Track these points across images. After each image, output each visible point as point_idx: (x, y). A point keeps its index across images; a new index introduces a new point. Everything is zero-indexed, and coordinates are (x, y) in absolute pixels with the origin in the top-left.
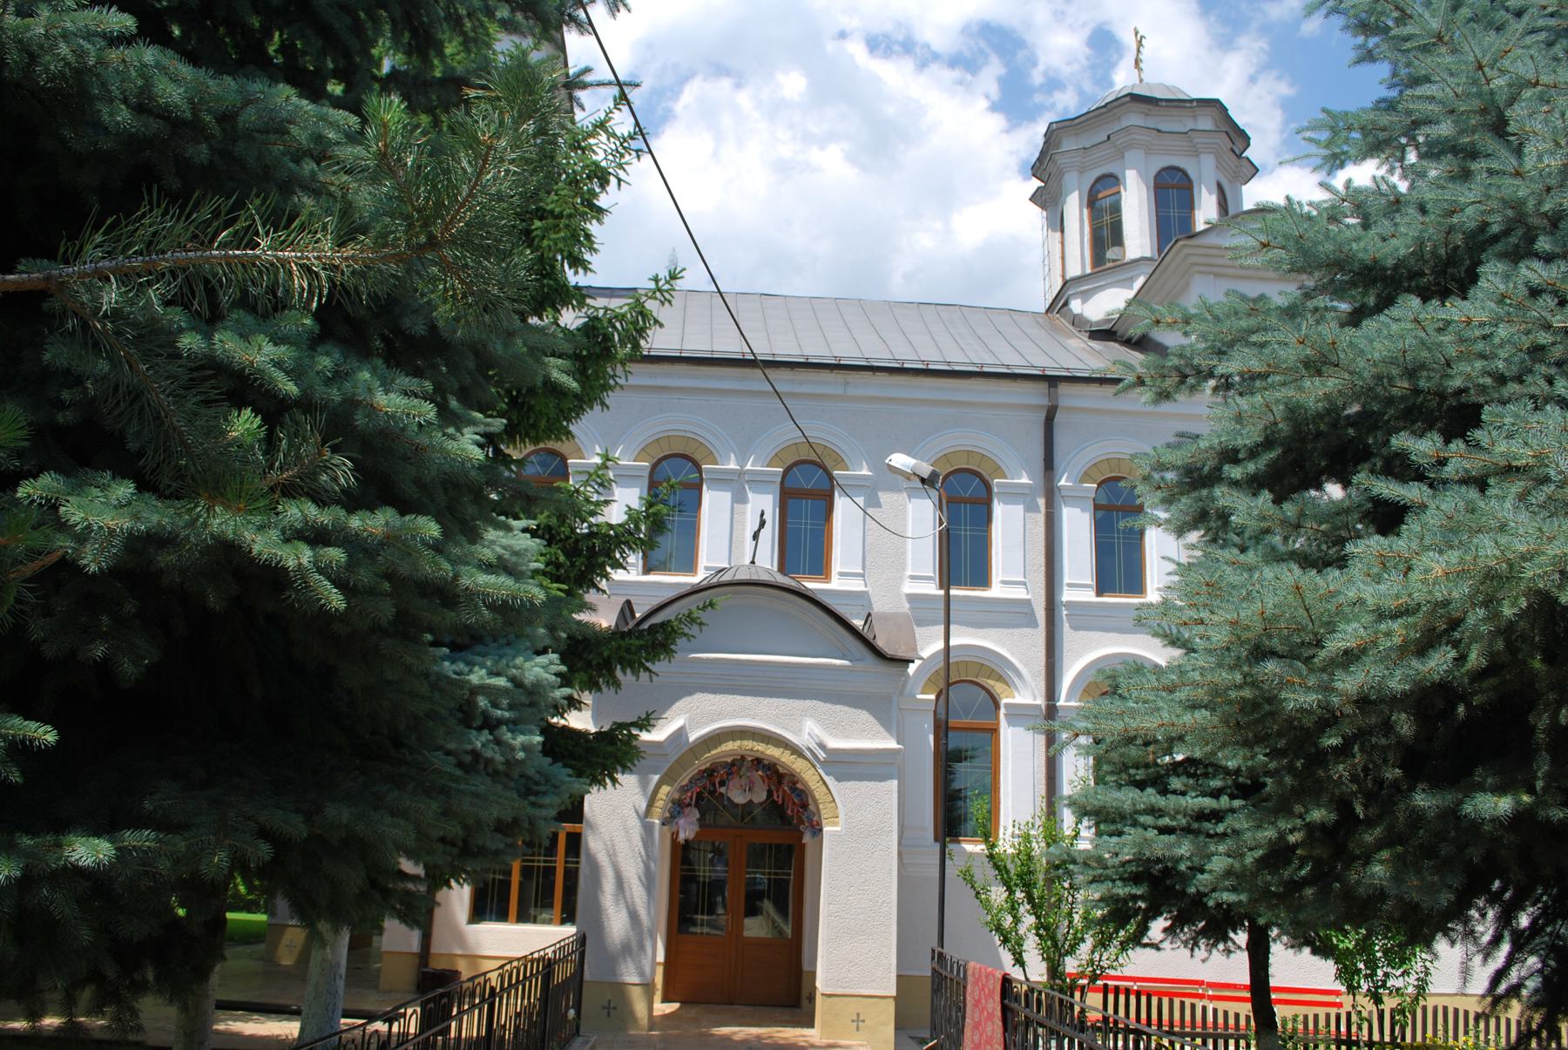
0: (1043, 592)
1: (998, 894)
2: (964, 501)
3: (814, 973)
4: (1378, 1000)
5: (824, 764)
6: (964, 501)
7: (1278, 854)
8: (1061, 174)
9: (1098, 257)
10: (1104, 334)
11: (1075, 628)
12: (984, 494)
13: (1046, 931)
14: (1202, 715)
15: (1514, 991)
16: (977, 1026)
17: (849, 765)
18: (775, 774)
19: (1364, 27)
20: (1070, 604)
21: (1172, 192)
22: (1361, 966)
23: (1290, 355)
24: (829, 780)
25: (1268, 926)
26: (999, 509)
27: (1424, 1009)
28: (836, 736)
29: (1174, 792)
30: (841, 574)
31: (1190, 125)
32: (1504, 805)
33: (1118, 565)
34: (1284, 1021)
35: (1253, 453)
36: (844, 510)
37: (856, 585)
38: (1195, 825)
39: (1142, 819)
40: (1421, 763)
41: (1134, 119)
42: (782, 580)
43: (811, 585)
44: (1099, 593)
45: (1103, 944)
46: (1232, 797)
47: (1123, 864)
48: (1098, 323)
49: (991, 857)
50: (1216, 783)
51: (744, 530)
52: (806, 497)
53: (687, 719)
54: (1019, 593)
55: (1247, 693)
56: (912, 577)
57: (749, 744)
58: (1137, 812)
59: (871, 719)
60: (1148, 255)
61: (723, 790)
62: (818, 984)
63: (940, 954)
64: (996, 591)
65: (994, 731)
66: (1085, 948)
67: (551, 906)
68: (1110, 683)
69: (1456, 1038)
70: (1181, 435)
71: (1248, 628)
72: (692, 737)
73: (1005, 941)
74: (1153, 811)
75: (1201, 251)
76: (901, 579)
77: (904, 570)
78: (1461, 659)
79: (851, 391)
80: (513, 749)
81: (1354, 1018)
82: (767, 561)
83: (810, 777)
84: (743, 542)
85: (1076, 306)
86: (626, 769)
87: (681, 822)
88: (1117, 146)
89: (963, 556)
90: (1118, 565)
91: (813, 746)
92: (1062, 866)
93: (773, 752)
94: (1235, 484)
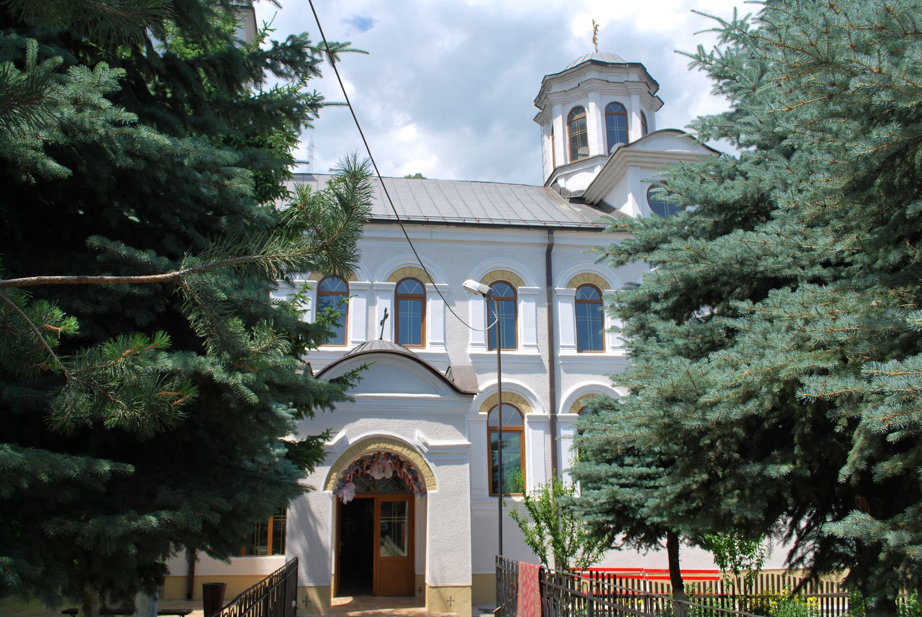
0: (547, 351)
1: (531, 525)
2: (502, 301)
3: (423, 577)
4: (737, 572)
5: (427, 454)
6: (502, 301)
7: (684, 495)
8: (552, 106)
9: (574, 154)
10: (578, 199)
11: (567, 372)
12: (512, 295)
13: (557, 543)
14: (644, 431)
15: (801, 559)
16: (525, 596)
17: (442, 456)
18: (398, 462)
19: (718, 76)
20: (563, 358)
21: (616, 117)
22: (727, 554)
23: (683, 254)
24: (431, 465)
25: (678, 533)
26: (522, 306)
27: (762, 576)
28: (433, 438)
29: (627, 465)
30: (432, 344)
31: (625, 78)
32: (785, 469)
33: (589, 336)
34: (688, 586)
35: (666, 296)
36: (433, 306)
37: (440, 350)
38: (639, 482)
39: (611, 480)
40: (747, 451)
41: (593, 74)
42: (398, 348)
43: (415, 350)
44: (579, 351)
45: (589, 549)
46: (657, 467)
47: (602, 504)
48: (575, 193)
49: (527, 504)
50: (649, 460)
51: (374, 319)
52: (410, 301)
53: (351, 433)
54: (534, 352)
55: (666, 420)
56: (473, 344)
57: (383, 445)
58: (609, 477)
59: (441, 425)
60: (602, 153)
61: (368, 472)
62: (427, 581)
63: (501, 559)
64: (521, 351)
65: (521, 432)
66: (579, 552)
67: (265, 544)
68: (594, 407)
69: (779, 591)
70: (630, 284)
71: (666, 391)
72: (351, 442)
73: (536, 550)
74: (616, 475)
75: (633, 154)
76: (466, 345)
77: (468, 340)
78: (761, 405)
79: (435, 237)
80: (273, 457)
81: (725, 583)
82: (389, 340)
83: (419, 462)
84: (373, 326)
85: (561, 183)
86: (319, 463)
87: (345, 491)
88: (584, 90)
89: (501, 333)
90: (589, 336)
91: (421, 445)
92: (568, 508)
93: (397, 449)
94: (656, 312)
